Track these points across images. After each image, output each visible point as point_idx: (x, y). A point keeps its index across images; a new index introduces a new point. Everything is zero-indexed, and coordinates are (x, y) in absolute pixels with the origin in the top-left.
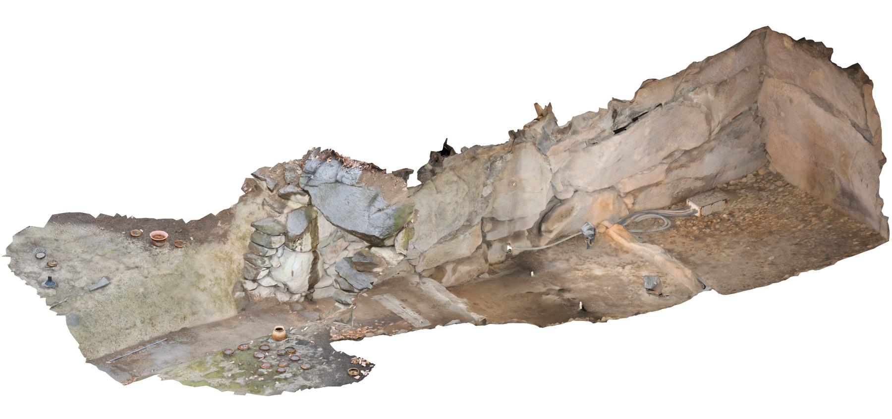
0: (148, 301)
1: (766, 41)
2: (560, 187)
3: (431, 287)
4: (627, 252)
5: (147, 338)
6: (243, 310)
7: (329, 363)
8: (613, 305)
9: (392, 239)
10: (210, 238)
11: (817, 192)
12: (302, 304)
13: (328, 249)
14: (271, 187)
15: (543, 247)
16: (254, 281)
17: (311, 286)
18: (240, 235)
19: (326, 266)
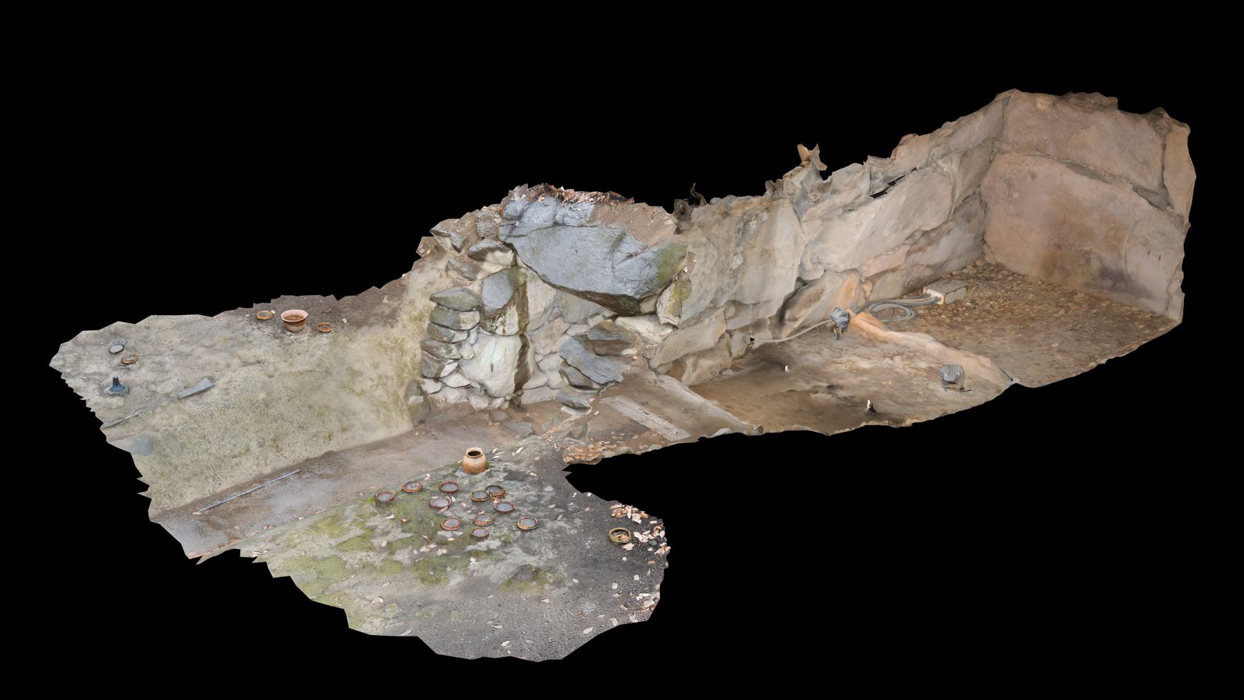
0: (272, 411)
1: (1008, 108)
2: (809, 266)
3: (671, 384)
4: (886, 343)
5: (268, 470)
6: (422, 422)
7: (568, 516)
8: (905, 404)
9: (652, 302)
10: (372, 319)
11: (1057, 278)
12: (506, 411)
13: (541, 333)
14: (458, 245)
15: (784, 339)
16: (437, 379)
17: (519, 387)
18: (415, 313)
19: (539, 358)
